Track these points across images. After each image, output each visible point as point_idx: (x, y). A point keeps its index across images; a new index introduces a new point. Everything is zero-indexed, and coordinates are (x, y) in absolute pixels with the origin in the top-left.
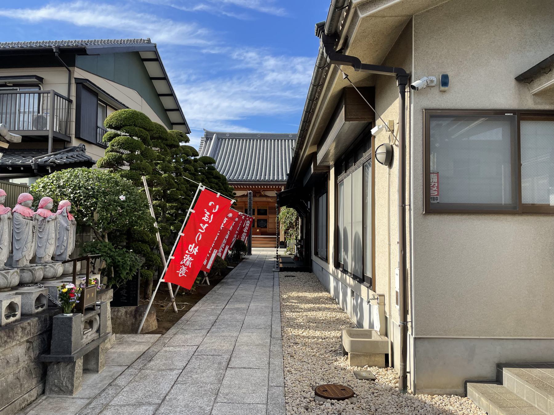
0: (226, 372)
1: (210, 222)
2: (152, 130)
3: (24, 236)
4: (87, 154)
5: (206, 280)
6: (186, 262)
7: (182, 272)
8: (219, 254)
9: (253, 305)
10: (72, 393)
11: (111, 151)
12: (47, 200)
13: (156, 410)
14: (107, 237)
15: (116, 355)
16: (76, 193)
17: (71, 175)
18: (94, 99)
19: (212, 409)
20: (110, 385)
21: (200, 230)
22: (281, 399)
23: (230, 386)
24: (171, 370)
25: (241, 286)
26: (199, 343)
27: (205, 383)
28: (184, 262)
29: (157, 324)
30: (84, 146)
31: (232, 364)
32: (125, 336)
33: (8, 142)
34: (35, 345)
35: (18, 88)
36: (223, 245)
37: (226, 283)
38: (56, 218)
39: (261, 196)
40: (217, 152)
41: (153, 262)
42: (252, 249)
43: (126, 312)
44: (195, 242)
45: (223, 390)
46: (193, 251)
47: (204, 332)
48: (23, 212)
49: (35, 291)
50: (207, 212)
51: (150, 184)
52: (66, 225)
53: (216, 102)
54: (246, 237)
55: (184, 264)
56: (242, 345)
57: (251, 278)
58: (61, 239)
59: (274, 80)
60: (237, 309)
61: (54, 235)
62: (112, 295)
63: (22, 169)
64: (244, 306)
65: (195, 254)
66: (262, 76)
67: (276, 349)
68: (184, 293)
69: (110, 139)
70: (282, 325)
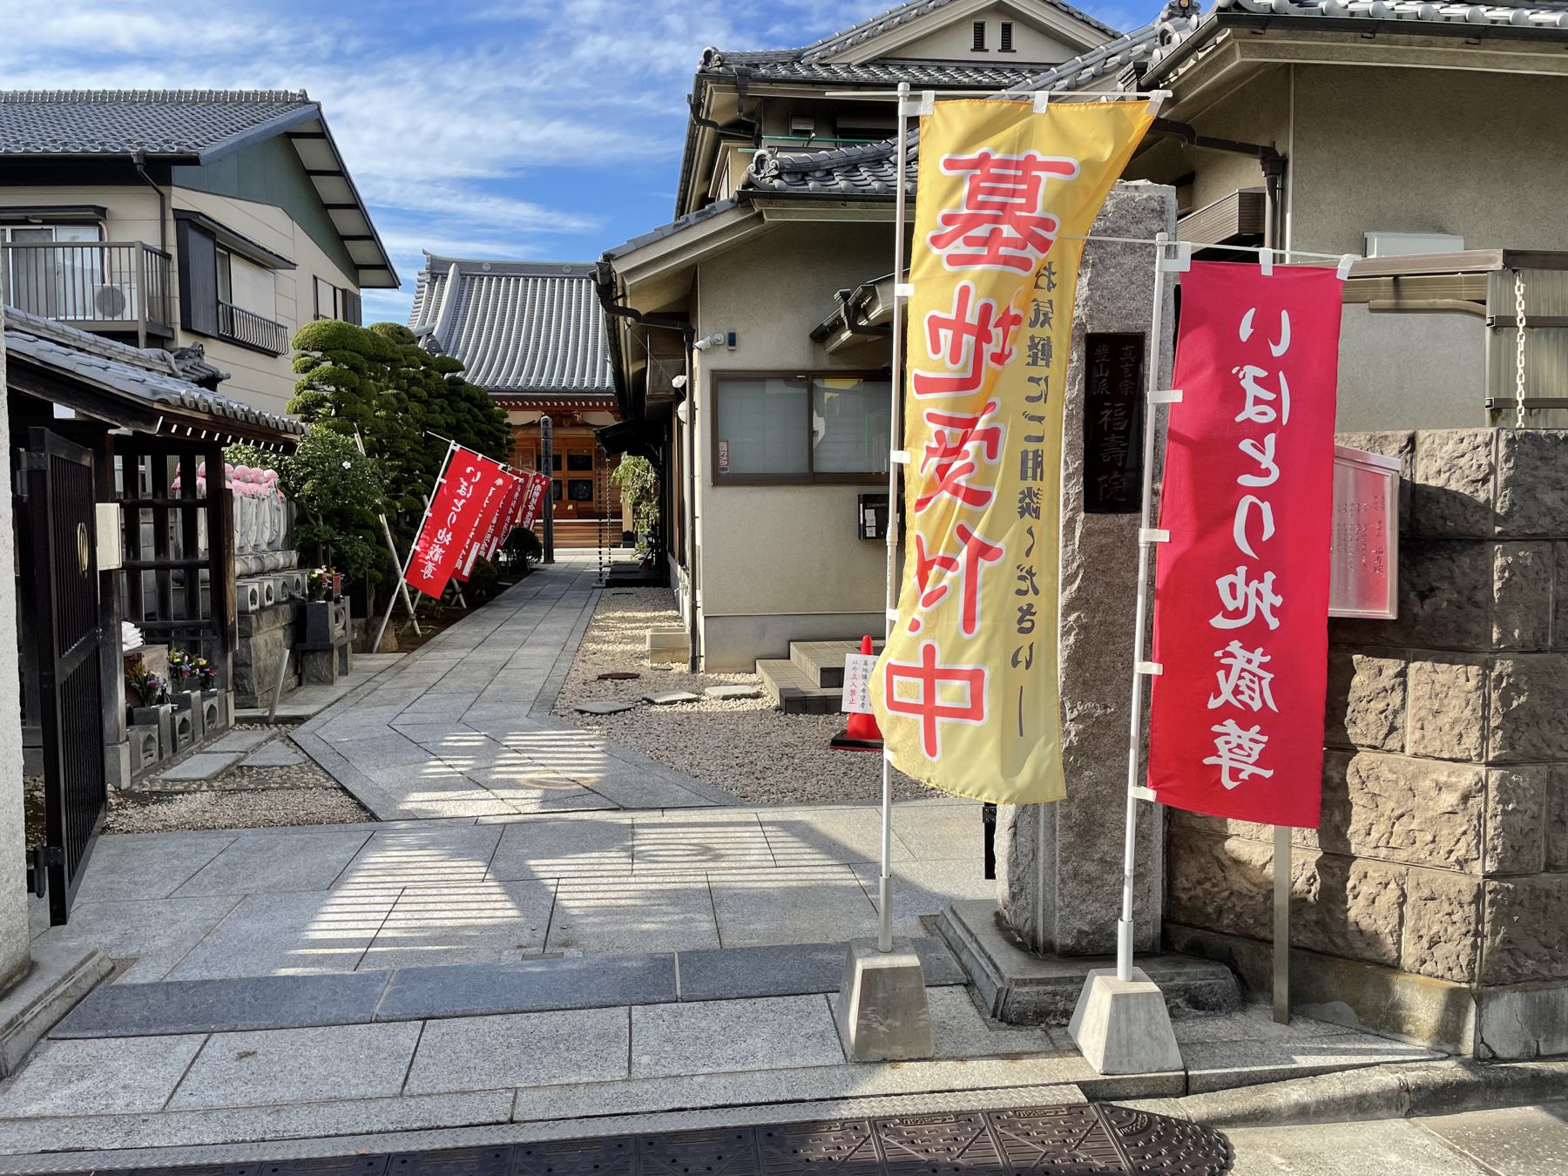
4: (207, 361)
5: (459, 600)
8: (482, 554)
36: (489, 536)
39: (575, 425)
57: (545, 597)
59: (604, 60)
66: (563, 45)
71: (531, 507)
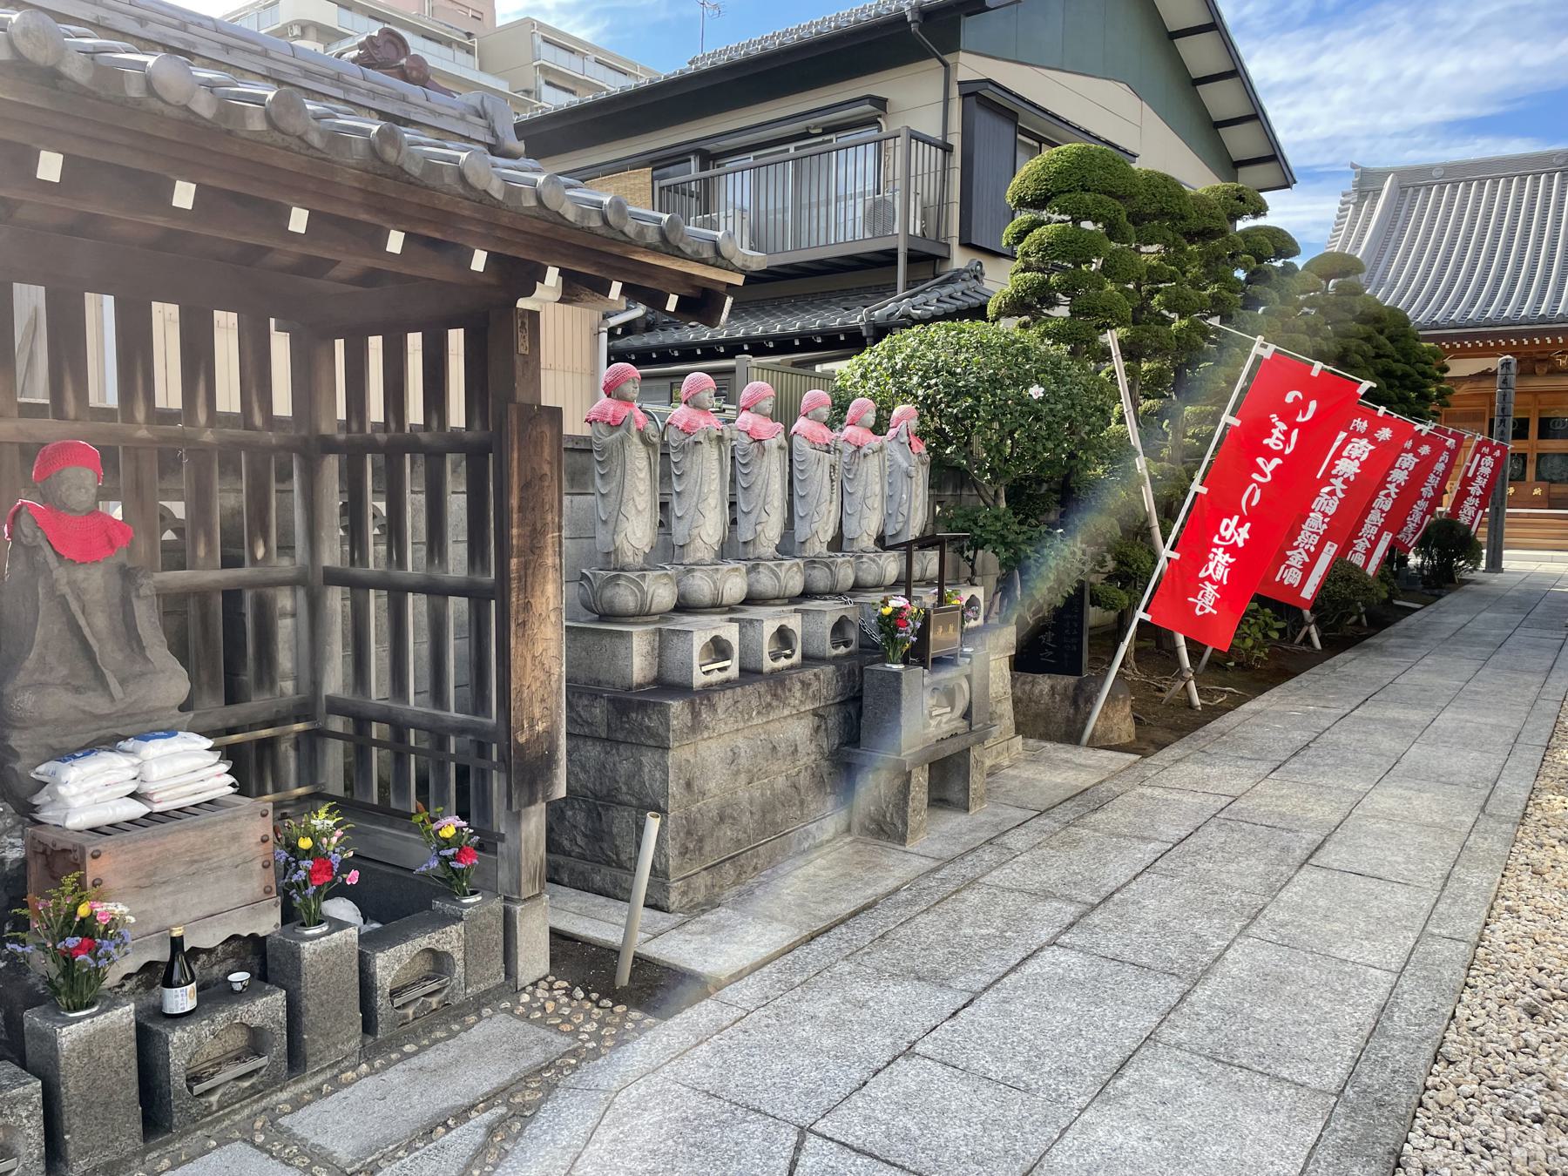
0: (1297, 872)
1: (1287, 451)
2: (1132, 196)
3: (814, 488)
6: (1215, 570)
7: (1206, 600)
9: (1447, 719)
10: (905, 841)
11: (1023, 271)
12: (861, 406)
13: (1081, 917)
14: (1003, 495)
15: (1017, 783)
16: (929, 387)
17: (921, 342)
18: (1007, 130)
19: (1228, 947)
20: (990, 842)
21: (1255, 476)
22: (1450, 972)
23: (1298, 908)
24: (1143, 839)
25: (1428, 661)
26: (1240, 792)
27: (1228, 887)
28: (1211, 571)
29: (1133, 730)
30: (980, 264)
31: (1322, 858)
32: (1049, 745)
33: (742, 271)
34: (830, 724)
35: (833, 136)
37: (1380, 649)
38: (881, 449)
40: (1395, 234)
41: (1131, 567)
42: (1505, 552)
43: (1053, 688)
44: (1240, 513)
45: (1276, 914)
46: (1233, 535)
47: (1264, 767)
48: (812, 436)
49: (831, 611)
50: (1278, 424)
51: (1131, 352)
52: (905, 465)
53: (1411, 66)
54: (1476, 513)
55: (1209, 578)
56: (1373, 817)
58: (896, 498)
60: (1393, 723)
61: (877, 488)
62: (1013, 639)
63: (842, 338)
64: (1415, 715)
65: (1241, 544)
67: (1488, 844)
68: (1232, 664)
69: (1020, 236)
70: (1537, 785)
71: (1475, 490)
